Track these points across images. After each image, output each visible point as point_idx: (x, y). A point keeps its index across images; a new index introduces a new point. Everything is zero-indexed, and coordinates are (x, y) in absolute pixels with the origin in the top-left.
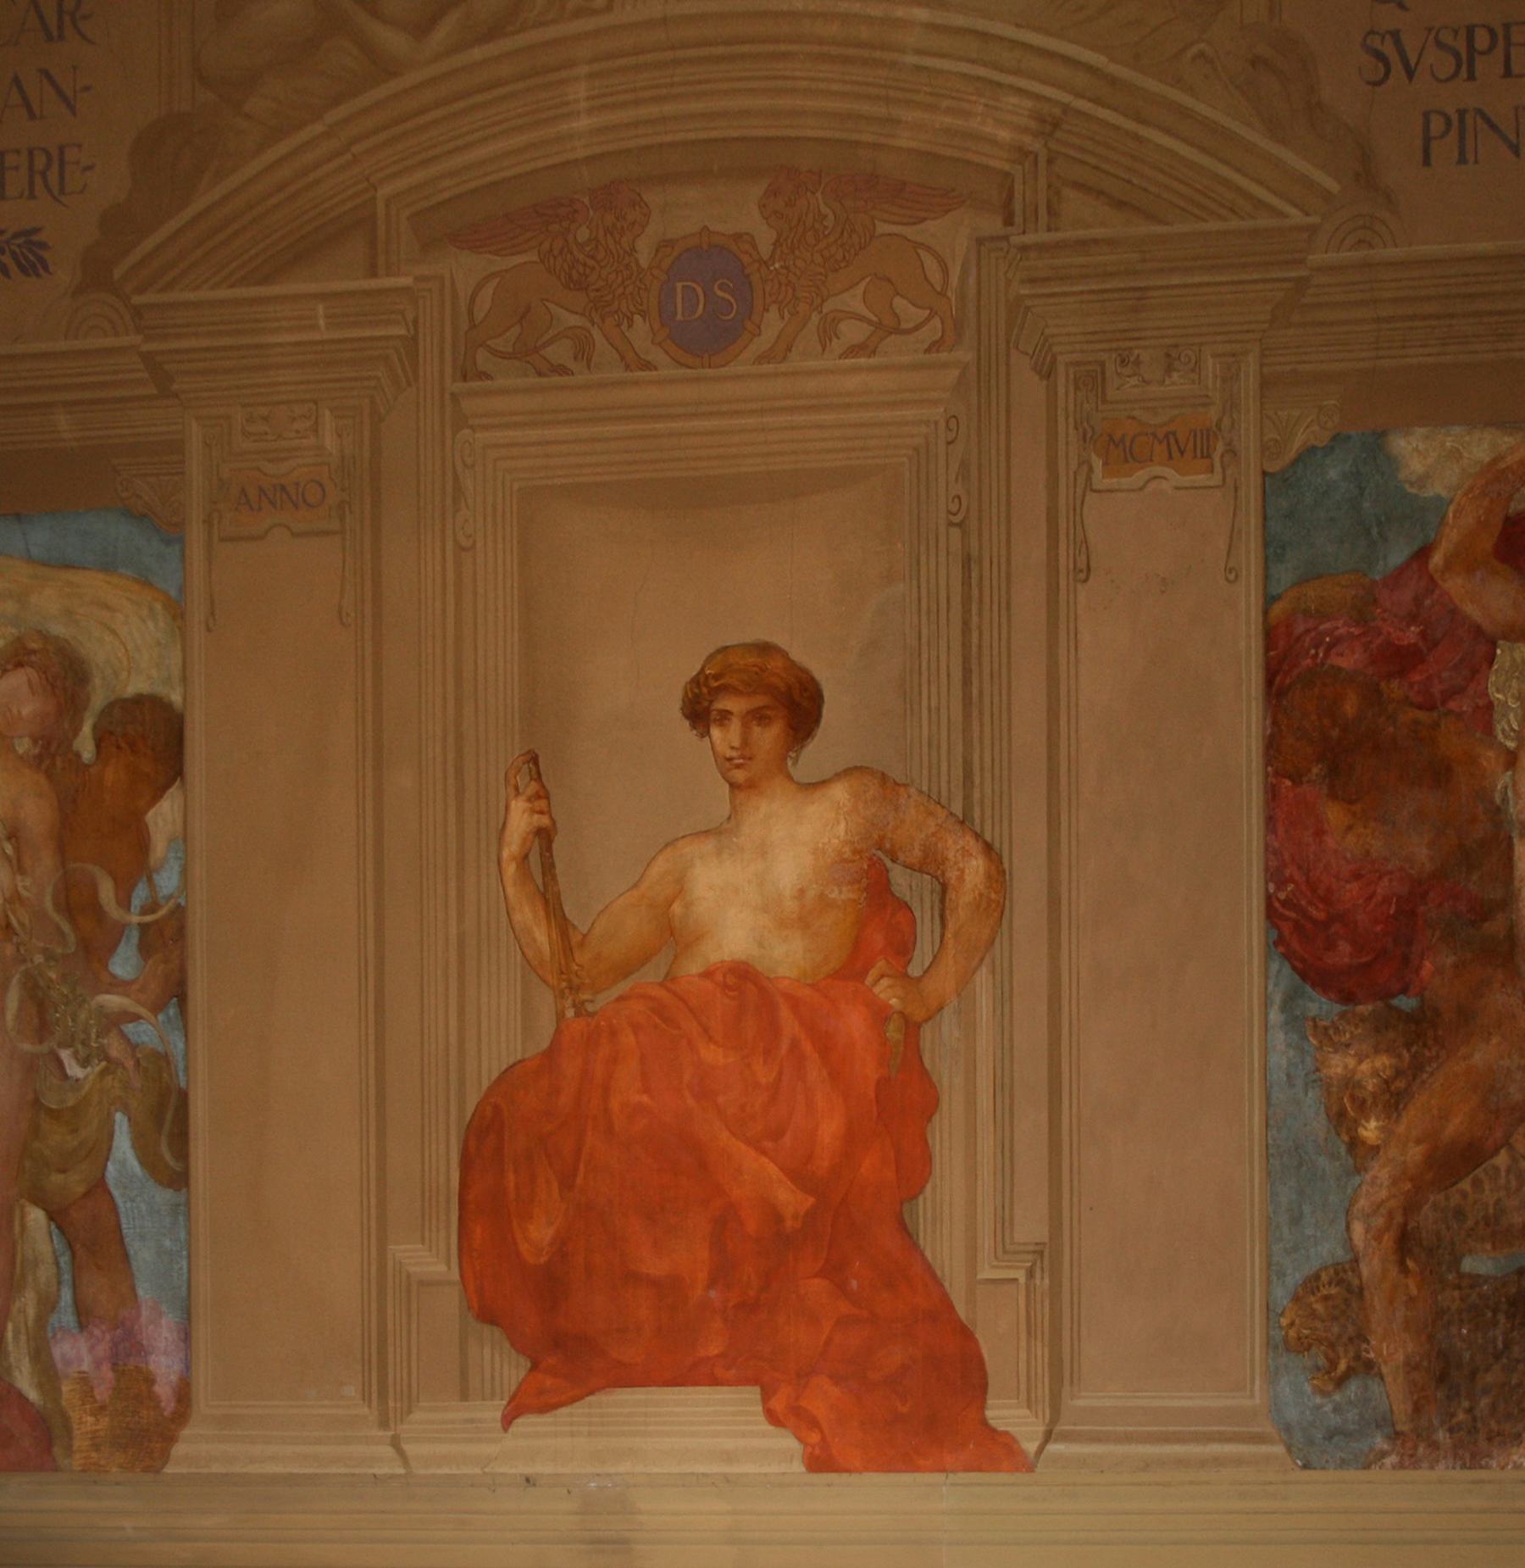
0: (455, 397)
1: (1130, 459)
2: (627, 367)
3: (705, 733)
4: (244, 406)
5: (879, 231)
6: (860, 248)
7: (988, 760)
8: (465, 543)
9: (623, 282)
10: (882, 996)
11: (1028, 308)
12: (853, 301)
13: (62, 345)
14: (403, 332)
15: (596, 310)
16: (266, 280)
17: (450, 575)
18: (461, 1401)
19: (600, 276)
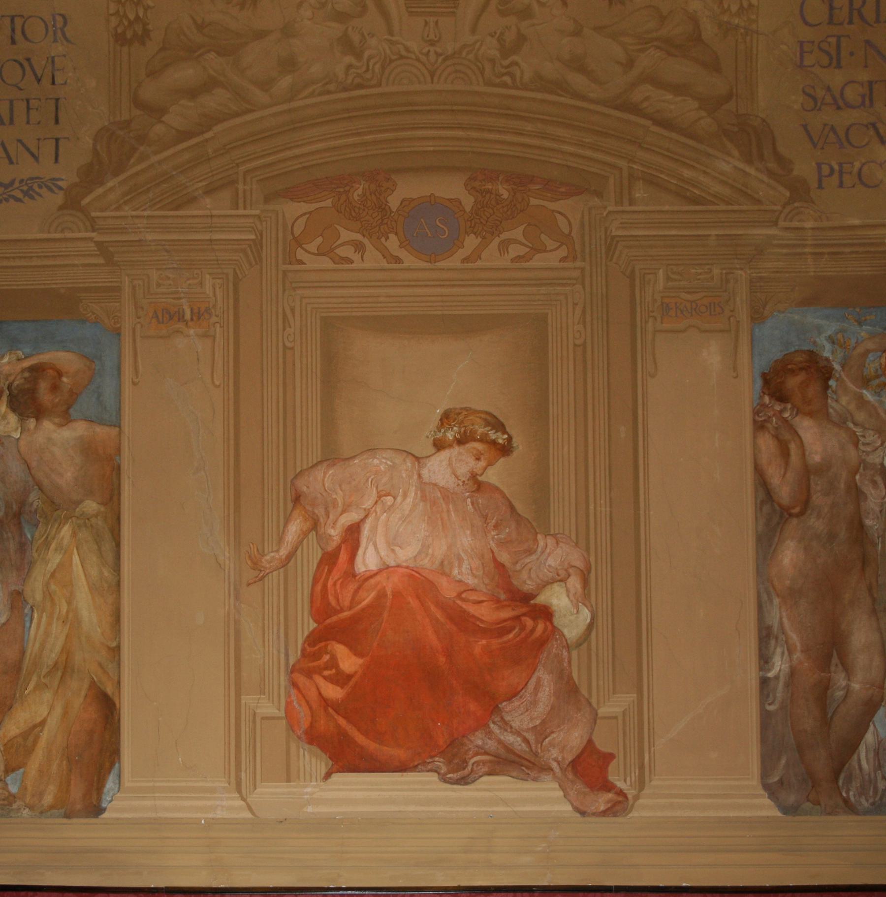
0: (285, 273)
1: (845, 144)
2: (388, 263)
3: (760, 671)
4: (158, 269)
5: (531, 203)
6: (521, 211)
7: (271, 586)
8: (289, 345)
9: (381, 218)
10: (491, 435)
11: (618, 242)
12: (518, 233)
13: (58, 236)
14: (253, 237)
15: (366, 230)
16: (177, 208)
17: (281, 360)
18: (287, 782)
19: (367, 213)
